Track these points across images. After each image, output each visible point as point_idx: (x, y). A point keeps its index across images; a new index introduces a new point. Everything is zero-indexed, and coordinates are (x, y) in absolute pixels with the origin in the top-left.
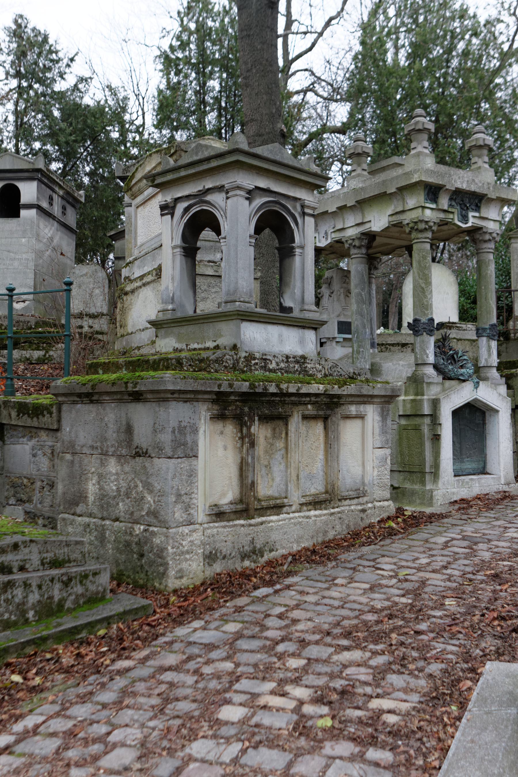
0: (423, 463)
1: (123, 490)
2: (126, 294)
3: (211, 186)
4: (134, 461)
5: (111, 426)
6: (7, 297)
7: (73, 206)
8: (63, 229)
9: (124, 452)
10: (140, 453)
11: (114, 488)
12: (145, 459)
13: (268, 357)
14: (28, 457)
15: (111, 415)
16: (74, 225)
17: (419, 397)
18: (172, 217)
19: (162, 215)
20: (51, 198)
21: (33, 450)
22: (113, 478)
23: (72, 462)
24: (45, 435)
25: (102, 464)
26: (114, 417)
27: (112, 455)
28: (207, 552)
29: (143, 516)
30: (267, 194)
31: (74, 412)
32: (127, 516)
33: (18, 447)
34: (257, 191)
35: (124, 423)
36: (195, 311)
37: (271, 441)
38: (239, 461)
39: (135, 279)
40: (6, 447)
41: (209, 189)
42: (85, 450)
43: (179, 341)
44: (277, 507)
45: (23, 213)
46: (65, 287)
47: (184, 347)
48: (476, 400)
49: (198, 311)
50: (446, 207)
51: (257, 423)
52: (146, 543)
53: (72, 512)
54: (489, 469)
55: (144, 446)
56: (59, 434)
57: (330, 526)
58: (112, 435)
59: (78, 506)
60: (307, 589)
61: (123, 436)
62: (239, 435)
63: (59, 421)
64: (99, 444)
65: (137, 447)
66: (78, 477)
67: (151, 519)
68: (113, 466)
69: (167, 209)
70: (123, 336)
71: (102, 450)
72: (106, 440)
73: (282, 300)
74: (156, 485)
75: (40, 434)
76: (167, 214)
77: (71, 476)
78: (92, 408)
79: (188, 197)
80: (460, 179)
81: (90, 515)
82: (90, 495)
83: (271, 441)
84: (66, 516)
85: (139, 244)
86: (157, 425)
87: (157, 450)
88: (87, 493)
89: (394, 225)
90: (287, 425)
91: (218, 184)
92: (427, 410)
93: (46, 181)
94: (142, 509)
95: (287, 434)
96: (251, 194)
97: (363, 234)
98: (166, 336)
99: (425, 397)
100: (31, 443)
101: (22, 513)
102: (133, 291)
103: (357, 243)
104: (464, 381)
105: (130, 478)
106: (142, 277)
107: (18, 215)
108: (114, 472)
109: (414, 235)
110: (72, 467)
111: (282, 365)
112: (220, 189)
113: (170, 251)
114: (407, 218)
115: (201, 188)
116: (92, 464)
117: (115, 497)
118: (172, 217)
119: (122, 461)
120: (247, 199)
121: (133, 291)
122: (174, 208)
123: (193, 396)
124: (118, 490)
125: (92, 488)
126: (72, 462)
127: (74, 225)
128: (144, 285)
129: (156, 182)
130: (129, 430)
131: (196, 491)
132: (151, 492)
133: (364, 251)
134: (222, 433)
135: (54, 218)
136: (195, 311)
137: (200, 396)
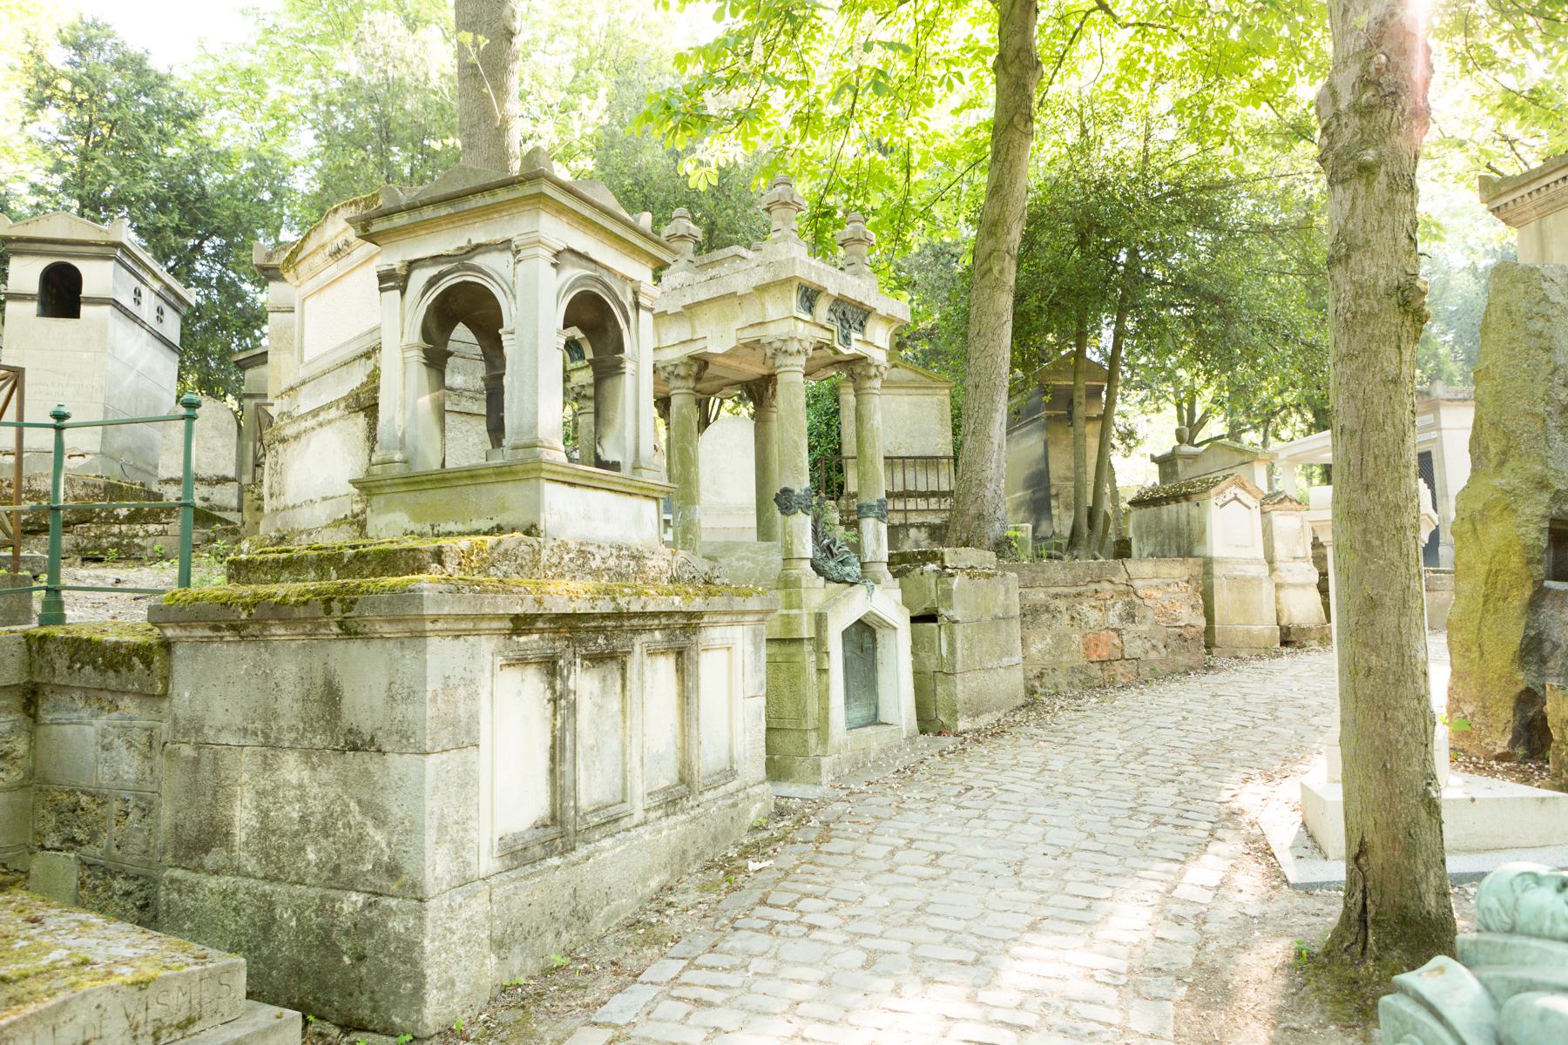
0: (802, 714)
1: (314, 821)
2: (283, 441)
3: (483, 240)
4: (341, 759)
5: (287, 686)
6: (53, 431)
7: (176, 310)
8: (157, 344)
9: (318, 741)
10: (357, 744)
11: (295, 815)
12: (366, 756)
13: (591, 549)
14: (92, 751)
15: (288, 663)
16: (176, 341)
17: (794, 612)
18: (403, 294)
19: (382, 290)
20: (138, 293)
21: (104, 736)
22: (291, 794)
23: (196, 762)
24: (132, 706)
25: (267, 765)
26: (295, 670)
27: (290, 748)
28: (497, 933)
29: (364, 874)
30: (584, 263)
31: (201, 658)
32: (325, 874)
33: (70, 730)
34: (568, 255)
35: (319, 681)
36: (443, 465)
37: (599, 700)
38: (549, 743)
39: (302, 417)
40: (41, 731)
41: (478, 246)
42: (226, 738)
43: (416, 517)
44: (611, 822)
45: (84, 309)
46: (183, 411)
47: (428, 529)
48: (870, 614)
49: (448, 465)
50: (824, 322)
51: (578, 669)
52: (370, 931)
53: (194, 863)
54: (882, 718)
55: (366, 729)
56: (166, 705)
57: (689, 841)
58: (289, 707)
59: (207, 852)
60: (707, 994)
61: (315, 710)
62: (548, 694)
63: (166, 679)
64: (259, 725)
65: (350, 731)
66: (205, 784)
67: (383, 882)
68: (292, 769)
69: (392, 280)
70: (276, 511)
71: (266, 736)
72: (276, 715)
73: (599, 450)
74: (395, 809)
75: (121, 704)
76: (392, 288)
77: (193, 789)
78: (247, 652)
79: (436, 259)
80: (835, 282)
81: (238, 871)
82: (236, 831)
83: (599, 700)
84: (178, 873)
85: (306, 359)
86: (395, 687)
87: (396, 737)
88: (230, 825)
89: (745, 345)
90: (623, 669)
91: (498, 237)
92: (807, 630)
93: (129, 263)
94: (362, 858)
95: (624, 686)
96: (562, 256)
97: (692, 358)
98: (388, 508)
99: (805, 611)
100: (102, 721)
101: (74, 865)
102: (297, 437)
103: (682, 371)
104: (852, 584)
105: (332, 795)
106: (315, 413)
107: (75, 314)
108: (294, 782)
109: (781, 360)
110: (195, 772)
111: (612, 562)
112: (506, 245)
113: (398, 355)
114: (772, 332)
115: (463, 243)
116: (244, 771)
117: (296, 834)
118: (403, 294)
119: (315, 759)
120: (554, 265)
121: (297, 437)
122: (406, 278)
123: (471, 625)
124: (303, 819)
125: (242, 817)
126: (196, 762)
127: (176, 341)
128: (321, 425)
129: (373, 229)
130: (331, 696)
131: (474, 815)
132: (380, 823)
133: (691, 383)
134: (519, 693)
135: (142, 324)
136: (443, 465)
137: (484, 625)
